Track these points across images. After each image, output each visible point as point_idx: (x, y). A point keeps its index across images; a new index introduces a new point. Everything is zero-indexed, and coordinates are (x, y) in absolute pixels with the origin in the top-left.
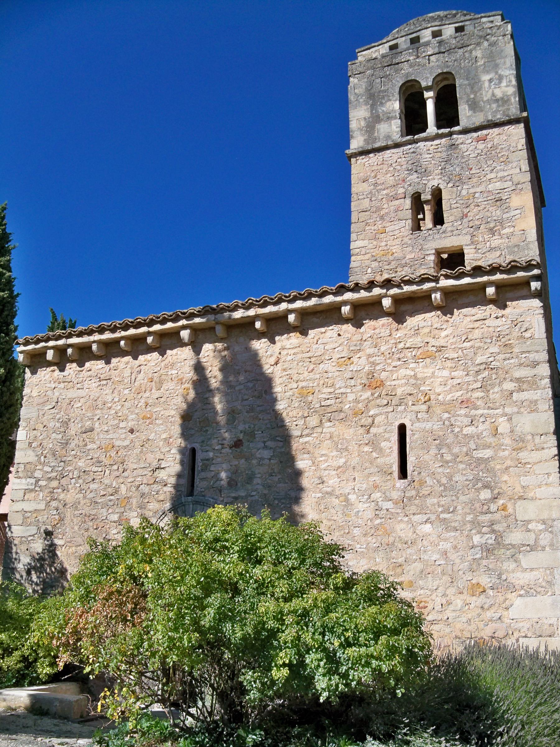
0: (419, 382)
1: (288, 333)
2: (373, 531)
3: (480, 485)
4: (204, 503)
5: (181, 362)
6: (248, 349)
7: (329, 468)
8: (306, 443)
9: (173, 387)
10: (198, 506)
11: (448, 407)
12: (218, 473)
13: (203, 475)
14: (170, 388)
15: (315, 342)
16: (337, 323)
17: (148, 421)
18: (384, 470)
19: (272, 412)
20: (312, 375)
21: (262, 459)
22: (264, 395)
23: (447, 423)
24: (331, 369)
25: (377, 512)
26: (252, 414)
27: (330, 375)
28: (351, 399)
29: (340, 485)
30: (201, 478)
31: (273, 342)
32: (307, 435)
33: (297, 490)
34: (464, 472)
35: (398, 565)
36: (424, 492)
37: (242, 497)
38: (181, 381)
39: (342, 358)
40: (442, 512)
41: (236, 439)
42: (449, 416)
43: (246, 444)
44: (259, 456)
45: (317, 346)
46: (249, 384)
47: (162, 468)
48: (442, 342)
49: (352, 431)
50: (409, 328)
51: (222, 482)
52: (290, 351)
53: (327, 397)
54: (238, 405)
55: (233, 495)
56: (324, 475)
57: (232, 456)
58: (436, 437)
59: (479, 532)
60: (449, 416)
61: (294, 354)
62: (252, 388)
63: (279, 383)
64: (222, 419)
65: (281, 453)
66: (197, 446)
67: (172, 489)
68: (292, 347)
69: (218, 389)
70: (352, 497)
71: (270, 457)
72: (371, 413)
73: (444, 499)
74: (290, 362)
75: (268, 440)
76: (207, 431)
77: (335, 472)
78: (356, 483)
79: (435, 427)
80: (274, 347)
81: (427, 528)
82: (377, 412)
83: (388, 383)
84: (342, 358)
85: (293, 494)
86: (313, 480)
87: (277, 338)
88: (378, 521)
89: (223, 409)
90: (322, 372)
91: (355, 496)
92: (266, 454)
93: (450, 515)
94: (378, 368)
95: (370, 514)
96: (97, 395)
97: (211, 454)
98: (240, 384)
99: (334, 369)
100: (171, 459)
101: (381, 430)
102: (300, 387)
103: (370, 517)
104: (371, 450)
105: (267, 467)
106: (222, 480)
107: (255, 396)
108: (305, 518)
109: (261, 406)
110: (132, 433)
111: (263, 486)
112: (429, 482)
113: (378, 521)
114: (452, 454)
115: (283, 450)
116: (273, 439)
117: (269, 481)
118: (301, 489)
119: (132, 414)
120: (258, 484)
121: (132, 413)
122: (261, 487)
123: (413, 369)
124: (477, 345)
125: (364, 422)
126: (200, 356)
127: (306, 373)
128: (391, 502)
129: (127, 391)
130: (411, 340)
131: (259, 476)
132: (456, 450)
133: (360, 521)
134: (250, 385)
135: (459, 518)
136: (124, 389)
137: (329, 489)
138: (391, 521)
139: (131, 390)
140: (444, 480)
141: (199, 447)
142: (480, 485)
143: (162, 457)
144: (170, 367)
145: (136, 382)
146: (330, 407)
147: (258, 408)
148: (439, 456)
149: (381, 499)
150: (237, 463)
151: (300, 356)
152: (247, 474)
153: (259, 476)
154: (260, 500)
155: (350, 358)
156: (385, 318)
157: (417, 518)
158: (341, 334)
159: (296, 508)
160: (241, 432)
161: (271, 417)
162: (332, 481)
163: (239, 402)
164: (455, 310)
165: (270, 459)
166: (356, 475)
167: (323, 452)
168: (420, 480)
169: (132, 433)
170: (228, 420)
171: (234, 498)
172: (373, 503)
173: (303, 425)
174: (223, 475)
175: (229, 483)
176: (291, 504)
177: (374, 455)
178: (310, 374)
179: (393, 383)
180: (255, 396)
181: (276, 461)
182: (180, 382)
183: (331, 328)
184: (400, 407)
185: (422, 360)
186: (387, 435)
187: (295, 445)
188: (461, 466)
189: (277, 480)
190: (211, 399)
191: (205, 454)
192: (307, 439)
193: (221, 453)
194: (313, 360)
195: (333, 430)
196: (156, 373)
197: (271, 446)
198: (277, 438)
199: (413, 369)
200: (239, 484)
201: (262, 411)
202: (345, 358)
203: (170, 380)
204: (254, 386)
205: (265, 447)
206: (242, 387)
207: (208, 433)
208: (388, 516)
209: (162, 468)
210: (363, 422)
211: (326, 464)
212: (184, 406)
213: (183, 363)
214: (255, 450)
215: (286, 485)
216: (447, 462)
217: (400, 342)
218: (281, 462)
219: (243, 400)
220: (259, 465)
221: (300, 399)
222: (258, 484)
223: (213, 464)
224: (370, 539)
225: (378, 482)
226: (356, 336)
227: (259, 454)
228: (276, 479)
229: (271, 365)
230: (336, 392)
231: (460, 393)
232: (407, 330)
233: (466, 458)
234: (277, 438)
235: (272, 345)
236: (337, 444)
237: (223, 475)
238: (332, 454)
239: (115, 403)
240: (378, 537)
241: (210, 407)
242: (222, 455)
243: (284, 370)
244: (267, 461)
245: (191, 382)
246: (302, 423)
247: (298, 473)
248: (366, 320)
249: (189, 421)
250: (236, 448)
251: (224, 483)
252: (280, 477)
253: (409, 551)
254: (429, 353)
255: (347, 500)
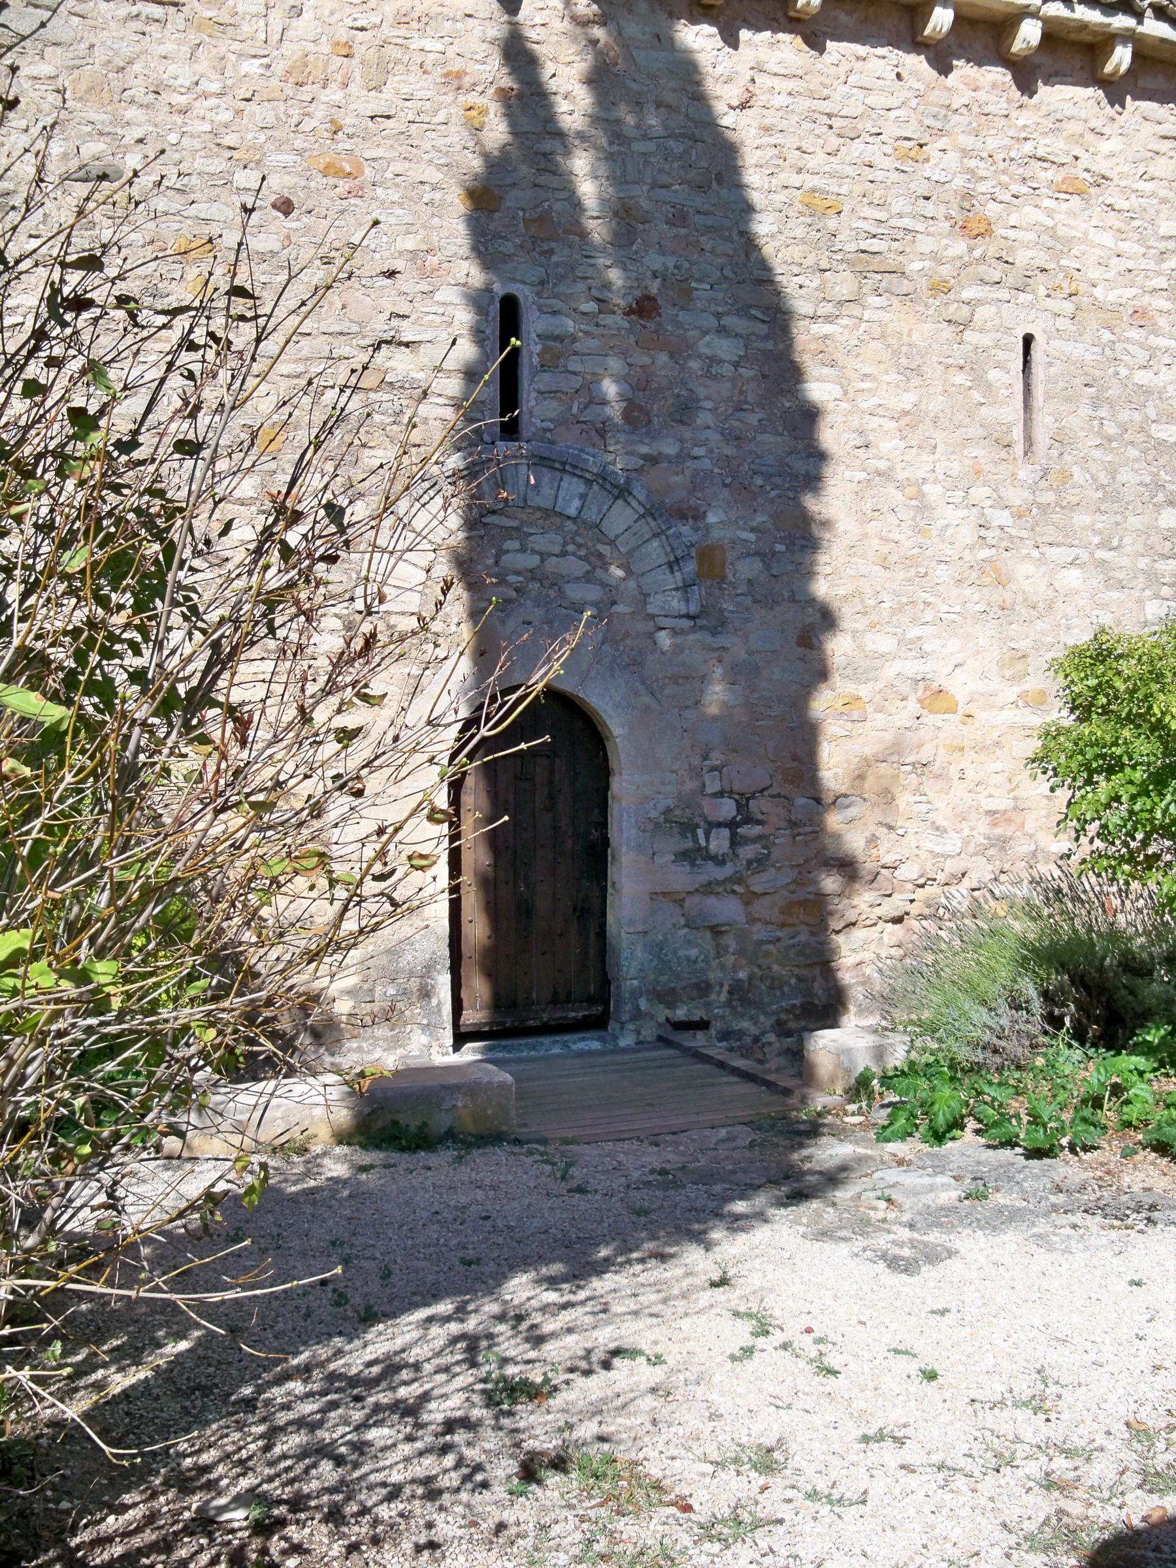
0: (1059, 246)
1: (775, 31)
2: (974, 575)
3: (1160, 498)
4: (564, 464)
5: (455, 20)
6: (664, 41)
7: (881, 411)
8: (826, 337)
9: (429, 94)
10: (544, 470)
11: (1110, 315)
12: (597, 379)
13: (545, 380)
14: (419, 94)
15: (843, 78)
16: (895, 42)
17: (344, 185)
18: (995, 435)
19: (736, 238)
20: (834, 164)
21: (714, 360)
22: (714, 184)
23: (1108, 351)
24: (878, 160)
25: (983, 532)
26: (683, 231)
27: (879, 175)
28: (927, 251)
29: (905, 457)
30: (542, 389)
31: (732, 41)
32: (829, 319)
33: (808, 457)
34: (1136, 466)
35: (1020, 654)
36: (1070, 498)
37: (669, 459)
38: (455, 81)
39: (906, 139)
40: (1098, 546)
41: (638, 293)
42: (1113, 338)
43: (668, 311)
44: (708, 351)
45: (846, 88)
46: (671, 143)
47: (400, 344)
48: (1103, 167)
49: (928, 327)
50: (1044, 110)
51: (608, 411)
52: (777, 83)
53: (873, 231)
54: (641, 196)
55: (644, 449)
56: (870, 427)
57: (632, 340)
58: (1089, 380)
59: (1157, 596)
60: (1113, 338)
61: (790, 94)
62: (681, 158)
63: (753, 162)
64: (597, 229)
65: (764, 352)
66: (524, 294)
67: (449, 413)
68: (783, 71)
69: (582, 136)
70: (933, 492)
71: (736, 358)
72: (967, 294)
73: (1103, 518)
74: (780, 114)
75: (728, 313)
76: (551, 252)
77: (892, 424)
78: (937, 456)
79: (1088, 357)
80: (735, 59)
81: (1072, 578)
82: (980, 295)
83: (1003, 232)
84: (906, 139)
85: (800, 466)
86: (846, 436)
87: (745, 34)
88: (985, 553)
89: (603, 201)
90: (859, 161)
91: (938, 489)
92: (726, 349)
93: (1112, 553)
94: (982, 187)
95: (967, 534)
96: (127, 50)
97: (570, 325)
98: (645, 137)
99: (888, 163)
100: (438, 319)
101: (986, 340)
102: (807, 187)
103: (968, 541)
104: (969, 384)
105: (728, 385)
106: (604, 402)
107: (688, 182)
108: (829, 530)
109: (706, 213)
110: (287, 213)
111: (722, 434)
112: (1079, 476)
113: (985, 553)
114: (1119, 425)
115: (769, 345)
116: (743, 311)
117: (736, 424)
118: (821, 456)
119: (279, 149)
120: (708, 427)
121: (280, 146)
122: (717, 437)
123: (1050, 213)
124: (1163, 193)
125: (954, 313)
126: (522, 16)
127: (821, 156)
128: (1006, 513)
129: (252, 67)
130: (1047, 141)
131: (709, 404)
132: (1124, 415)
133: (947, 550)
134: (677, 147)
135: (1125, 561)
136: (240, 55)
137: (882, 465)
138: (1008, 554)
139: (268, 66)
140: (1103, 478)
141: (531, 297)
142: (1160, 498)
143: (403, 309)
144: (414, 25)
145: (286, 44)
146: (878, 257)
147: (698, 219)
148: (1096, 422)
149: (989, 502)
150: (646, 360)
151: (804, 104)
152: (678, 396)
153: (709, 404)
154: (716, 470)
155: (921, 146)
156: (999, 69)
157: (1052, 553)
158: (904, 74)
159: (811, 503)
160: (655, 275)
161: (734, 250)
162: (889, 446)
163: (645, 188)
164: (1128, 98)
165: (736, 365)
166: (939, 437)
167: (867, 370)
168: (1062, 471)
169: (287, 213)
170: (616, 234)
171: (645, 457)
172: (974, 510)
173: (816, 289)
174: (610, 389)
175: (627, 415)
176: (795, 490)
177: (976, 396)
178: (832, 159)
179: (1012, 234)
180: (688, 182)
181: (752, 373)
182: (455, 83)
183: (880, 51)
184: (1022, 295)
185: (1067, 197)
186: (1002, 355)
187: (806, 336)
188: (1133, 453)
189: (755, 423)
190: (559, 158)
191: (551, 320)
192: (827, 329)
193: (597, 325)
194: (837, 123)
195: (885, 316)
196: (362, 29)
197: (739, 331)
198: (753, 312)
199: (1050, 213)
200: (655, 420)
201: (709, 230)
202: (912, 143)
203: (414, 68)
204: (686, 152)
205: (722, 331)
206: (651, 146)
207: (554, 259)
208: (1004, 544)
209: (400, 344)
210: (952, 311)
211: (874, 401)
212: (476, 164)
213: (459, 25)
214: (696, 333)
215: (779, 439)
216: (1110, 440)
217: (1026, 139)
218: (764, 377)
219: (655, 185)
220: (708, 375)
221: (809, 220)
222: (708, 427)
223: (575, 353)
224: (968, 592)
225: (983, 461)
226: (936, 92)
227: (708, 344)
228: (753, 419)
229: (731, 107)
230: (893, 222)
231: (1130, 292)
232: (1042, 113)
233: (1141, 437)
234: (753, 312)
235: (727, 49)
236: (896, 353)
237: (610, 389)
238: (887, 378)
239: (206, 96)
240: (985, 590)
241: (554, 182)
242: (601, 330)
243: (767, 129)
244: (727, 370)
245: (491, 91)
246: (814, 285)
247: (810, 415)
248: (958, 58)
249: (493, 211)
250: (641, 317)
251: (615, 411)
252: (760, 416)
253: (1040, 625)
254: (1078, 184)
255: (921, 495)
